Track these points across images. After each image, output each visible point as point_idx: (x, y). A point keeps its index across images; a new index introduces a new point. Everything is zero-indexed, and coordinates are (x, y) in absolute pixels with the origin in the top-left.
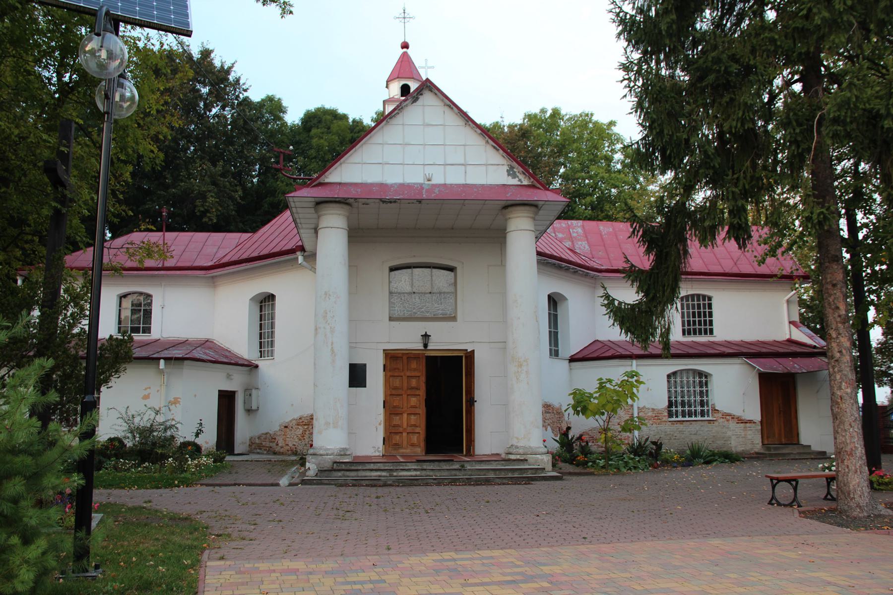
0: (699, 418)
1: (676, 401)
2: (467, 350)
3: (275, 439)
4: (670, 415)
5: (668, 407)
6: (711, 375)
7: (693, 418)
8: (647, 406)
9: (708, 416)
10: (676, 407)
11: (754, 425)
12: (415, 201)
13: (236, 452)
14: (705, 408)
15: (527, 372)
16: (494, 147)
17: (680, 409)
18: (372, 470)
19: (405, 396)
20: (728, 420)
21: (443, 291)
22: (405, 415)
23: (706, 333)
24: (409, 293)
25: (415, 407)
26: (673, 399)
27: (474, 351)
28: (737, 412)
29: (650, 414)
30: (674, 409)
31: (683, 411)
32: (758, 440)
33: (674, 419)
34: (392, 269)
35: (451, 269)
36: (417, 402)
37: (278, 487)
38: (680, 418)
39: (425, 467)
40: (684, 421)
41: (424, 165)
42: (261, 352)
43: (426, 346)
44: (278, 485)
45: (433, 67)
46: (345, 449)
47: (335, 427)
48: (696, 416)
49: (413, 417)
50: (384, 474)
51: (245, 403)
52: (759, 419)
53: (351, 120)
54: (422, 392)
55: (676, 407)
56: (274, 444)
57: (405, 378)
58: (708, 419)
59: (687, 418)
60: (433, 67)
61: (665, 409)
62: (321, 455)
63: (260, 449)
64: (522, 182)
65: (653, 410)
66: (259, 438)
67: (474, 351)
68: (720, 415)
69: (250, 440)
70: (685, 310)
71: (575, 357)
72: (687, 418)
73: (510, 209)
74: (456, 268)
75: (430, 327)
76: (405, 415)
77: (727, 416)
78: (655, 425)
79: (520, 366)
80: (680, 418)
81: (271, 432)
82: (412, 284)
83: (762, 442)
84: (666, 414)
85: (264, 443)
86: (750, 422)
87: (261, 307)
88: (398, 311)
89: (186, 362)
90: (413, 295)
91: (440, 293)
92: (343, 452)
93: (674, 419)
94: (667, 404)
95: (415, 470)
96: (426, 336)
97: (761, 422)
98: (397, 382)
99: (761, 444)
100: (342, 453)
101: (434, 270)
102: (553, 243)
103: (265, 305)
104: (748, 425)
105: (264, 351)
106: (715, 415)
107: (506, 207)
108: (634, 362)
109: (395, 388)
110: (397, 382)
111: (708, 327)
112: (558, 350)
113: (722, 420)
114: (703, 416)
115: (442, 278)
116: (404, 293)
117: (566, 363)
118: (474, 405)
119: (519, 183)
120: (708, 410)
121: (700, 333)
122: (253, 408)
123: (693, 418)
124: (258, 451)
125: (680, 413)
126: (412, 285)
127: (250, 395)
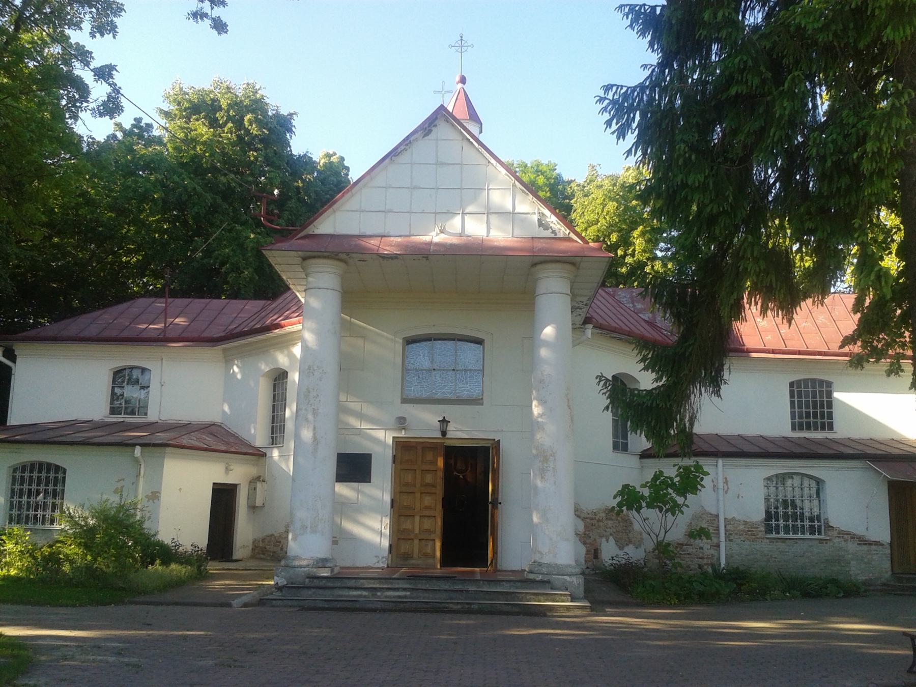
0: (807, 536)
1: (777, 513)
2: (494, 439)
3: (280, 542)
4: (769, 530)
5: (766, 520)
6: (824, 481)
7: (800, 536)
8: (738, 517)
9: (778, 533)
10: (777, 520)
11: (880, 547)
12: (420, 257)
13: (234, 557)
14: (816, 524)
15: (554, 469)
16: (523, 191)
17: (781, 523)
18: (350, 588)
19: (418, 495)
20: (846, 541)
21: (470, 367)
22: (417, 518)
23: (823, 428)
24: (429, 371)
25: (428, 508)
26: (773, 510)
27: (499, 440)
28: (860, 531)
29: (742, 527)
30: (773, 522)
31: (786, 526)
32: (887, 565)
33: (774, 535)
34: (410, 341)
35: (479, 342)
36: (433, 503)
37: (225, 610)
38: (782, 535)
39: (419, 586)
40: (787, 539)
41: (435, 213)
42: (272, 438)
43: (444, 433)
44: (229, 605)
45: (435, 92)
46: (325, 560)
47: (314, 531)
48: (803, 533)
49: (425, 520)
50: (365, 593)
51: (248, 499)
52: (889, 540)
53: (85, 49)
54: (439, 490)
55: (802, 521)
56: (279, 549)
57: (418, 472)
58: (820, 537)
59: (791, 536)
60: (435, 92)
61: (761, 522)
62: (294, 567)
63: (263, 554)
64: (556, 235)
65: (746, 523)
66: (263, 540)
67: (499, 440)
68: (835, 533)
69: (253, 542)
70: (796, 399)
71: (648, 452)
72: (791, 536)
73: (539, 267)
74: (484, 340)
75: (449, 411)
76: (417, 518)
77: (842, 534)
78: (747, 542)
79: (546, 460)
80: (782, 535)
81: (276, 534)
82: (433, 360)
83: (892, 570)
84: (763, 529)
85: (268, 547)
86: (877, 543)
87: (275, 385)
88: (414, 391)
89: (168, 449)
90: (434, 373)
91: (466, 370)
92: (322, 563)
93: (774, 535)
94: (763, 516)
95: (404, 589)
96: (444, 422)
97: (891, 544)
98: (409, 478)
99: (890, 573)
100: (320, 565)
101: (459, 343)
102: (628, 317)
103: (279, 383)
104: (873, 547)
105: (276, 437)
106: (830, 533)
107: (534, 265)
108: (720, 461)
109: (407, 484)
110: (409, 478)
111: (826, 420)
112: (627, 444)
113: (837, 540)
114: (812, 533)
115: (469, 354)
116: (422, 370)
117: (636, 459)
118: (497, 508)
119: (553, 235)
120: (820, 527)
121: (816, 429)
122: (257, 505)
123: (800, 536)
124: (262, 556)
125: (781, 529)
126: (432, 361)
127: (255, 489)
